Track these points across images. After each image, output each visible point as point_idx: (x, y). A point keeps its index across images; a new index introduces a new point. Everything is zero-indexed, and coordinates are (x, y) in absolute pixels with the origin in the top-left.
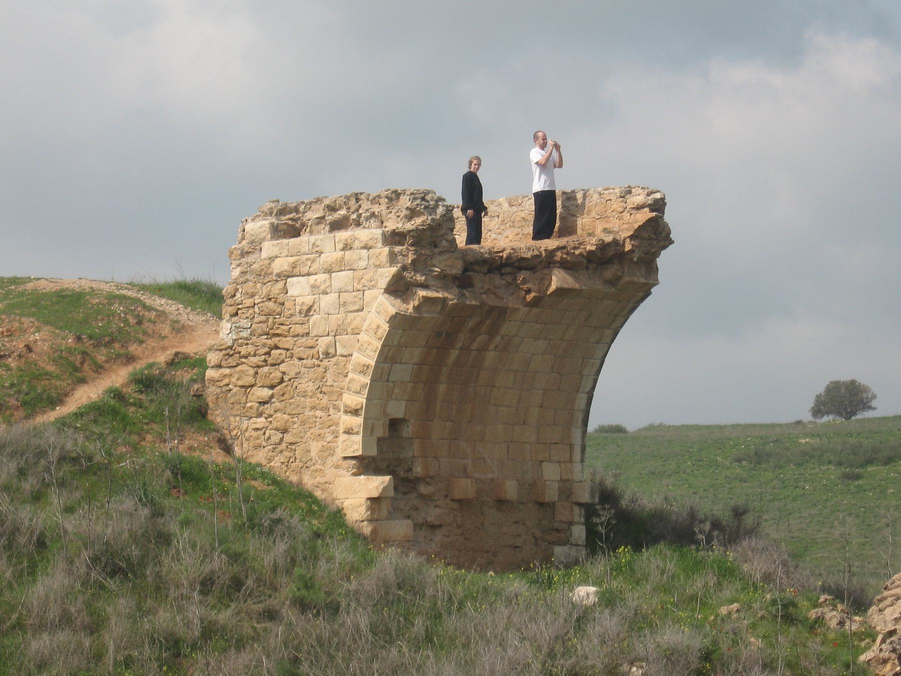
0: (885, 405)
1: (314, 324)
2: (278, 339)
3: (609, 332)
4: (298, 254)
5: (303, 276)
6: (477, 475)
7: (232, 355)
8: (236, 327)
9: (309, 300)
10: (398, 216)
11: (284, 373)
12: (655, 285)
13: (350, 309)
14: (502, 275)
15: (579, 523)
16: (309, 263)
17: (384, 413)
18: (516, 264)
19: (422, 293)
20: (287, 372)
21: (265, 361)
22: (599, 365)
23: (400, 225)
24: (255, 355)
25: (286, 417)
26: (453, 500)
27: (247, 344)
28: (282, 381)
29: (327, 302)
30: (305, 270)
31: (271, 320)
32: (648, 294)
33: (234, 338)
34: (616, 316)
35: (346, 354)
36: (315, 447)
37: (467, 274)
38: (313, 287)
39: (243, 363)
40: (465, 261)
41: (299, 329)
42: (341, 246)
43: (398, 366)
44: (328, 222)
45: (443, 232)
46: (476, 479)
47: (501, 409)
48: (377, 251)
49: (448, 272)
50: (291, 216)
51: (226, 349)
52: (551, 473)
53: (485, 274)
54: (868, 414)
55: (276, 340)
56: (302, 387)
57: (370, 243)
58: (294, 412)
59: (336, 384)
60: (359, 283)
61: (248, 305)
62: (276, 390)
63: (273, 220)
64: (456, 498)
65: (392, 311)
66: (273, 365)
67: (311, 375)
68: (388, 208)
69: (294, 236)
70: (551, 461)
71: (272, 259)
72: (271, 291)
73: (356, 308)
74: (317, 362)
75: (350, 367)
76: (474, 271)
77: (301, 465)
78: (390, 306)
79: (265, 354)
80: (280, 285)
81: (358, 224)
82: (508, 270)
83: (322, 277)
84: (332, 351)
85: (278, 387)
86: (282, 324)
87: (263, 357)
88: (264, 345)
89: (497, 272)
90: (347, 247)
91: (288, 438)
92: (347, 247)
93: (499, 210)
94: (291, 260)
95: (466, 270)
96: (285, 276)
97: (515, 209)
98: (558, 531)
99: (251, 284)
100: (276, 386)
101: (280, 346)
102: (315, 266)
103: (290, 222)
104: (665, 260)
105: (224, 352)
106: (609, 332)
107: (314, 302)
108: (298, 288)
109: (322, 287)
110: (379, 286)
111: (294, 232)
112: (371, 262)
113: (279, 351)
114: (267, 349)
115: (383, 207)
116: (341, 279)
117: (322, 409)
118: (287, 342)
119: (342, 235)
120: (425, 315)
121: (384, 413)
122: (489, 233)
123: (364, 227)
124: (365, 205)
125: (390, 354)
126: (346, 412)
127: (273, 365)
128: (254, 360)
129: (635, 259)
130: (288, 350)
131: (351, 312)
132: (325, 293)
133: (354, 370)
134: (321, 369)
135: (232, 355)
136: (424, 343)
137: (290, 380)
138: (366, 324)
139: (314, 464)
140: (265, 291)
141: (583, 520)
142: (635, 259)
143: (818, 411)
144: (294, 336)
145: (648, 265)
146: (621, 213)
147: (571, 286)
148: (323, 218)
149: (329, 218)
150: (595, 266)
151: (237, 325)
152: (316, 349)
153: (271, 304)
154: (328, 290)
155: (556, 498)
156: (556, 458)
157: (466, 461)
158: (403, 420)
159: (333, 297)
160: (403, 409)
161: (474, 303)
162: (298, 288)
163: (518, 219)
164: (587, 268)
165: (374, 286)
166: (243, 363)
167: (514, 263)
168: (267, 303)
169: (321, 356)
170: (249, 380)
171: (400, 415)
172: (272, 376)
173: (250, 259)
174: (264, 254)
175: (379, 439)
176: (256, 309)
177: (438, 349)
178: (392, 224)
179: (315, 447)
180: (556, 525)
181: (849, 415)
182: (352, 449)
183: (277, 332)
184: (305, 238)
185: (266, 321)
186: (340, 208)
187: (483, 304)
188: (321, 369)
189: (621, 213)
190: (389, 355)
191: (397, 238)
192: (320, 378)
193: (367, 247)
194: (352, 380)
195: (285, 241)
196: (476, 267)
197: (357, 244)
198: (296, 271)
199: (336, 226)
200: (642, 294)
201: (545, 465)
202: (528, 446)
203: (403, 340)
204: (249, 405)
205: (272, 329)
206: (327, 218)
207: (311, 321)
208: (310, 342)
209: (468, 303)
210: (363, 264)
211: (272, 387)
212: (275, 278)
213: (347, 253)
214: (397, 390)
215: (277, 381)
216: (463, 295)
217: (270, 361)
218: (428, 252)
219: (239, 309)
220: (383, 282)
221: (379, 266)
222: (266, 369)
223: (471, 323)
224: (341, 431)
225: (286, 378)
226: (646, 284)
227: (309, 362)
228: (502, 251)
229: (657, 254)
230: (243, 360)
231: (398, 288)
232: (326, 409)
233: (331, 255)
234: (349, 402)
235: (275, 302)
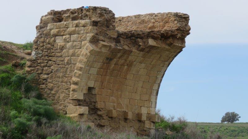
0: (242, 120)
1: (64, 53)
2: (51, 57)
3: (167, 63)
4: (60, 28)
5: (61, 36)
6: (118, 109)
7: (35, 63)
8: (37, 53)
9: (63, 44)
10: (95, 16)
11: (52, 69)
12: (185, 47)
13: (77, 48)
14: (131, 39)
15: (153, 129)
16: (63, 31)
17: (87, 85)
18: (136, 36)
19: (102, 43)
20: (54, 69)
21: (46, 65)
22: (162, 75)
23: (96, 19)
24: (43, 63)
25: (52, 85)
26: (109, 117)
27: (40, 59)
28: (52, 72)
29: (69, 45)
30: (62, 34)
31: (49, 51)
32: (181, 50)
33: (36, 57)
34: (170, 58)
35: (74, 63)
36: (62, 96)
37: (119, 38)
38: (65, 39)
39: (38, 66)
40: (118, 33)
41: (59, 54)
42: (74, 26)
43: (92, 68)
44: (71, 17)
45: (111, 22)
46: (118, 111)
47: (128, 87)
48: (87, 28)
49: (112, 36)
50: (58, 15)
51: (33, 61)
52: (144, 111)
53: (125, 39)
54: (237, 122)
55: (50, 58)
56: (58, 75)
57: (85, 25)
58: (55, 83)
59: (70, 74)
60: (80, 38)
61: (42, 45)
62: (49, 75)
63: (52, 16)
64: (110, 117)
65: (92, 48)
66: (49, 66)
67: (62, 70)
68: (92, 13)
69: (60, 22)
70: (144, 106)
71: (51, 30)
72: (50, 40)
73: (79, 47)
74: (64, 66)
75: (76, 68)
76: (121, 37)
77: (56, 101)
78: (91, 47)
79: (46, 63)
80: (53, 39)
81: (81, 19)
82: (133, 38)
83: (68, 36)
84: (69, 62)
85: (50, 74)
86: (53, 52)
87: (46, 64)
88: (46, 60)
89: (129, 38)
90: (77, 26)
91: (53, 92)
92: (77, 26)
93: (131, 19)
94: (57, 30)
95: (118, 37)
96: (55, 36)
97: (137, 19)
98: (145, 131)
99: (43, 38)
100: (49, 74)
101: (52, 60)
102: (66, 32)
103: (58, 17)
104: (188, 39)
105: (32, 62)
106: (167, 63)
107: (64, 45)
108: (60, 41)
109: (68, 40)
110: (87, 40)
111: (60, 20)
112: (85, 31)
113: (51, 62)
114: (46, 61)
115: (91, 13)
116: (74, 37)
117: (65, 82)
118: (54, 59)
119: (76, 22)
120: (103, 51)
121: (87, 85)
122: (128, 27)
123: (83, 20)
124: (84, 12)
125: (90, 64)
126: (73, 84)
127: (49, 66)
128: (42, 65)
129: (178, 37)
130: (54, 61)
131: (77, 49)
132: (68, 42)
133: (77, 69)
134: (65, 69)
135: (35, 63)
136: (102, 61)
137: (54, 72)
138: (82, 53)
139: (61, 102)
140: (48, 41)
141: (154, 128)
142: (178, 37)
143: (224, 120)
144: (57, 57)
145: (182, 40)
146: (174, 21)
147: (155, 45)
148: (69, 16)
149: (71, 16)
150: (164, 39)
151: (38, 52)
152: (64, 62)
153: (49, 46)
154: (70, 41)
155: (146, 120)
156: (146, 106)
157: (114, 104)
158: (93, 88)
159: (70, 43)
160: (93, 84)
161: (120, 48)
162: (60, 41)
163: (138, 22)
164: (161, 40)
165: (85, 40)
166: (38, 66)
167: (135, 35)
168: (48, 45)
169: (66, 64)
170: (40, 72)
171: (92, 86)
172: (48, 70)
173: (43, 29)
174: (48, 28)
175: (84, 94)
176: (44, 47)
177: (107, 63)
178: (94, 19)
179: (62, 96)
180: (145, 129)
181: (232, 122)
182: (74, 97)
183: (51, 55)
184: (64, 23)
185: (47, 51)
186: (75, 13)
187: (124, 49)
188: (65, 69)
189: (174, 21)
190: (90, 64)
191: (95, 24)
192: (65, 71)
193: (84, 26)
194: (76, 73)
195: (55, 24)
196: (122, 36)
197: (81, 25)
198: (59, 34)
199: (74, 19)
200: (179, 50)
201: (142, 107)
202: (136, 101)
203: (94, 60)
204: (40, 80)
205: (49, 54)
206: (71, 16)
207: (63, 51)
208: (62, 59)
209: (118, 48)
210: (82, 32)
211: (48, 74)
212: (51, 36)
213: (77, 28)
214: (91, 77)
215: (50, 72)
216: (117, 45)
217: (48, 65)
218: (105, 29)
219: (38, 47)
220: (88, 39)
221: (88, 33)
222: (46, 68)
223: (119, 55)
224: (71, 90)
225: (53, 71)
226: (181, 47)
227: (62, 66)
228: (131, 31)
229: (185, 37)
230: (39, 65)
231: (94, 41)
232: (66, 82)
233: (71, 29)
234: (74, 80)
235: (51, 45)
